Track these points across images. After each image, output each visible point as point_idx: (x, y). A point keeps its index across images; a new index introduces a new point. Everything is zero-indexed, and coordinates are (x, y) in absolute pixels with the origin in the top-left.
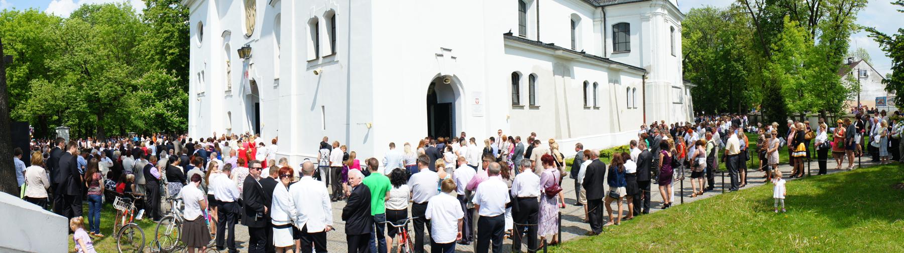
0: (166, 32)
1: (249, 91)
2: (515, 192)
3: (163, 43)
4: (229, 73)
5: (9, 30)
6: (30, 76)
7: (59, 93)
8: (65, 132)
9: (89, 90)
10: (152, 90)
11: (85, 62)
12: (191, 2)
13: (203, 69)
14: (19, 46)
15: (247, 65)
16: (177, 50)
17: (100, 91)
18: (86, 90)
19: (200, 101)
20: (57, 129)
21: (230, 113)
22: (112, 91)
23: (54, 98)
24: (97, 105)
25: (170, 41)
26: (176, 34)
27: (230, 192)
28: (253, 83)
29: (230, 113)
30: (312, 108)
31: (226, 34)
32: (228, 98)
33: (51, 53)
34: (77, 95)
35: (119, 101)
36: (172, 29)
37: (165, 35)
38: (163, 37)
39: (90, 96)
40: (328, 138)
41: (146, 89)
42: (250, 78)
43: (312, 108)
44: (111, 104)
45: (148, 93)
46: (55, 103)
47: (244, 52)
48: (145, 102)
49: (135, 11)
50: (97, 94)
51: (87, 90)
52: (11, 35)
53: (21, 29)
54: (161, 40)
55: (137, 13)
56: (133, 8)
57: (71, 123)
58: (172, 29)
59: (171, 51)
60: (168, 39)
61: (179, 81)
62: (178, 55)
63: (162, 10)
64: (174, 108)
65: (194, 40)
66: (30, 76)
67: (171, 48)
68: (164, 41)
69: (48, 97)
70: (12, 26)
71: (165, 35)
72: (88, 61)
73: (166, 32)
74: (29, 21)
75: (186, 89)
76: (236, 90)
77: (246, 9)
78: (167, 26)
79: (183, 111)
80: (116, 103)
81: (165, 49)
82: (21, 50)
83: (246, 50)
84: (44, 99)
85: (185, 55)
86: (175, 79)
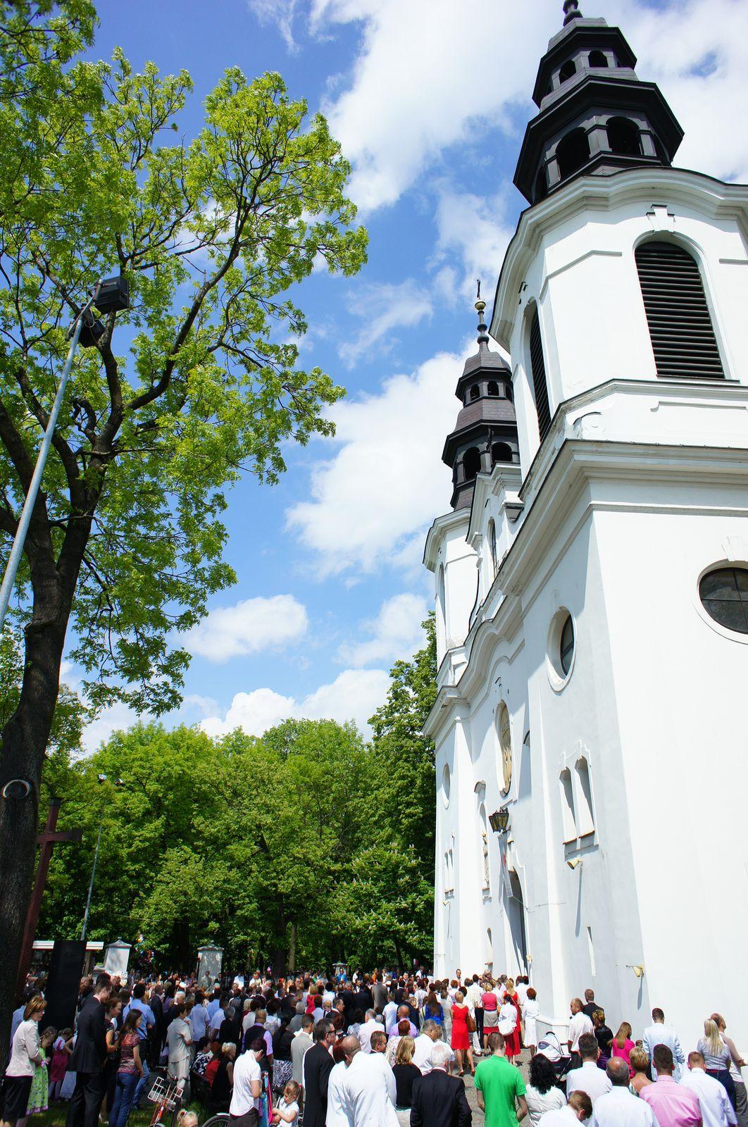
0: (403, 777)
1: (510, 894)
2: (289, 1119)
3: (397, 795)
4: (486, 855)
5: (141, 760)
6: (164, 842)
7: (209, 882)
8: (214, 958)
9: (263, 877)
10: (376, 880)
11: (259, 827)
12: (437, 731)
13: (451, 847)
14: (152, 786)
15: (505, 845)
16: (420, 809)
17: (280, 880)
18: (257, 878)
19: (448, 906)
20: (201, 951)
21: (489, 932)
22: (300, 882)
23: (200, 890)
24: (274, 906)
25: (408, 794)
26: (419, 782)
27: (698, 1101)
28: (514, 877)
29: (489, 932)
30: (577, 933)
31: (480, 788)
32: (487, 902)
33: (206, 803)
34: (241, 886)
35: (315, 901)
36: (413, 772)
37: (400, 782)
38: (397, 785)
39: (265, 889)
40: (593, 993)
41: (366, 878)
42: (510, 868)
43: (577, 933)
44: (301, 906)
45: (366, 886)
46: (200, 899)
47: (499, 821)
48: (365, 903)
49: (361, 740)
50: (275, 885)
51: (257, 878)
52: (143, 768)
53: (160, 759)
54: (394, 791)
55: (364, 742)
56: (358, 734)
57: (242, 937)
58: (413, 772)
59: (408, 811)
60: (405, 790)
61: (419, 865)
62: (419, 818)
63: (397, 741)
64: (405, 915)
65: (441, 794)
66: (164, 842)
67: (409, 805)
68: (398, 792)
69: (190, 889)
70: (147, 753)
71: (400, 782)
72: (264, 826)
73: (403, 777)
74: (177, 747)
75: (431, 880)
76: (495, 892)
77: (502, 750)
78: (403, 765)
79: (425, 921)
80: (309, 905)
81: (400, 807)
82: (156, 792)
83: (500, 818)
84: (181, 892)
85: (429, 820)
86: (414, 862)
